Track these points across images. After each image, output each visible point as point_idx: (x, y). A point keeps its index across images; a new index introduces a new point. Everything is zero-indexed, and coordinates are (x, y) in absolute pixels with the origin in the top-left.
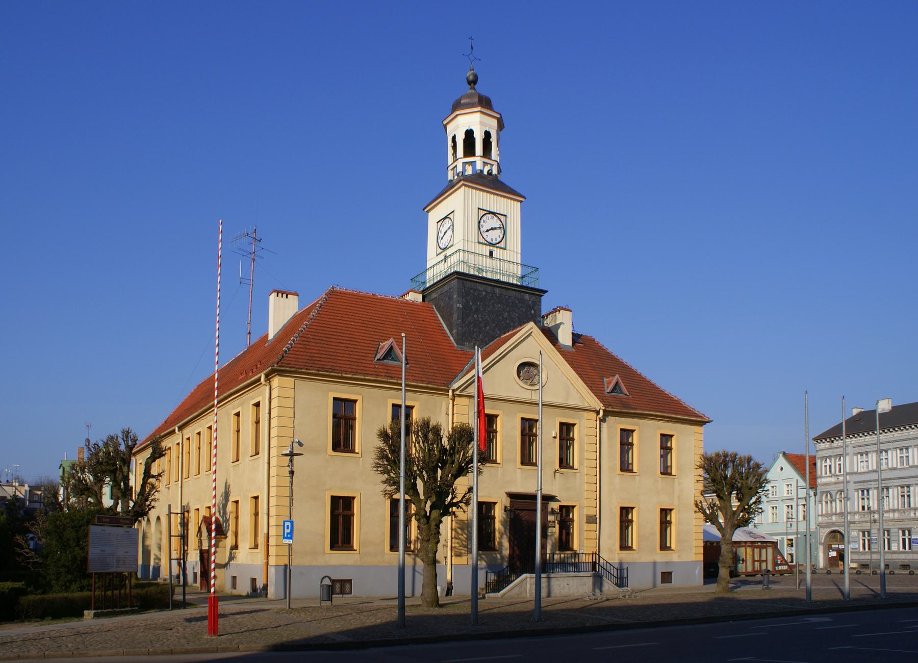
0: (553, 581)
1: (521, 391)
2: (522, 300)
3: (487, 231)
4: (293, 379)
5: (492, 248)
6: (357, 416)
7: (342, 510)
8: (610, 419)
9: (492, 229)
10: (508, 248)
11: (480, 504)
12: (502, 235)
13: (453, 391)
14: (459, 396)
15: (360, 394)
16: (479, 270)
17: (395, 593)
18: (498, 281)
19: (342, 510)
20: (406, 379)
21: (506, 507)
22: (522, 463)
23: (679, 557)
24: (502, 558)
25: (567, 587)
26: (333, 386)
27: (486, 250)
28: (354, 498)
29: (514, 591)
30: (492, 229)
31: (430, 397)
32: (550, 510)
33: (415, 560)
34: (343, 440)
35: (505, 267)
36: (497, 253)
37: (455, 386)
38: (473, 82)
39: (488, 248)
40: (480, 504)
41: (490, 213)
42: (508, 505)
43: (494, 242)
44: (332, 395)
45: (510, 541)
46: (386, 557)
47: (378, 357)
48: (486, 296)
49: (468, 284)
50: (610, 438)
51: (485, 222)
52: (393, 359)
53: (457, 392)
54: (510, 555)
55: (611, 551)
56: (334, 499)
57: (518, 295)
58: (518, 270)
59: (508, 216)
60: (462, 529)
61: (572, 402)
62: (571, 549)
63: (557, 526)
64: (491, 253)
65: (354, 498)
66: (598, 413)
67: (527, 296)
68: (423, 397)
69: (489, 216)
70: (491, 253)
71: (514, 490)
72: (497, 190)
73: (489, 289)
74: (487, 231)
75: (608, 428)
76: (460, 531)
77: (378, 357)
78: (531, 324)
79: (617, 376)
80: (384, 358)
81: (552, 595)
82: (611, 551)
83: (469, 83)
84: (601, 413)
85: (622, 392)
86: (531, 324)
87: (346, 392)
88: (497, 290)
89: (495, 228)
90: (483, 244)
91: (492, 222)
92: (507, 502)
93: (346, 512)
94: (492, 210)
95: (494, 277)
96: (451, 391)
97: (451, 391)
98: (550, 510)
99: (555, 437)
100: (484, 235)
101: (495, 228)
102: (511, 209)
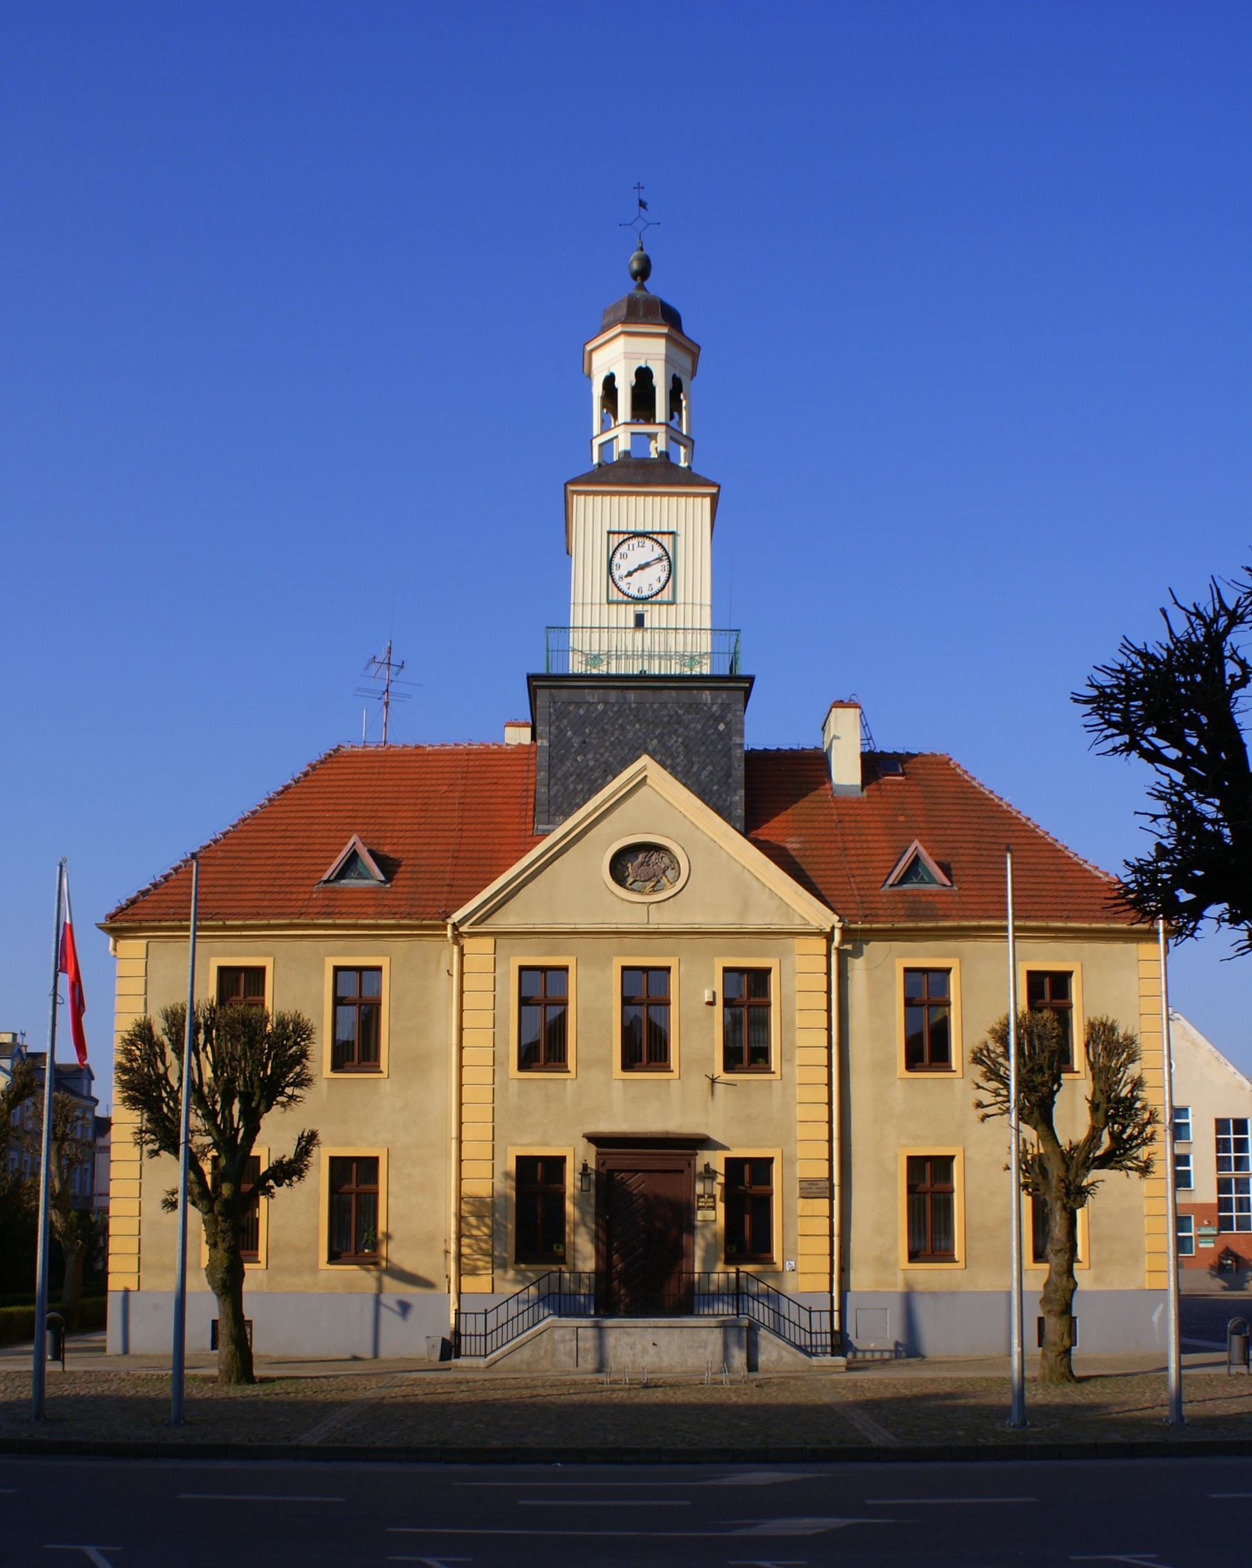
0: (612, 1338)
1: (625, 908)
2: (694, 707)
3: (630, 574)
4: (144, 942)
5: (639, 608)
6: (952, 999)
7: (929, 1181)
8: (874, 949)
9: (641, 567)
10: (680, 599)
11: (338, 1164)
12: (664, 576)
13: (455, 927)
14: (472, 935)
15: (267, 954)
16: (595, 659)
17: (168, 1346)
18: (643, 677)
19: (929, 1181)
20: (1015, 918)
21: (585, 1167)
22: (627, 1065)
23: (1097, 1279)
24: (577, 1275)
25: (652, 1350)
26: (219, 945)
27: (626, 615)
28: (952, 1158)
29: (517, 1357)
30: (641, 567)
31: (415, 943)
32: (700, 1168)
33: (379, 1280)
34: (927, 1048)
35: (677, 643)
36: (653, 616)
37: (457, 916)
38: (643, 273)
39: (631, 610)
40: (338, 1164)
41: (636, 535)
42: (592, 1165)
43: (646, 593)
44: (901, 964)
45: (596, 1239)
46: (322, 1275)
47: (890, 881)
48: (604, 712)
49: (564, 695)
50: (877, 991)
51: (623, 556)
52: (922, 881)
53: (463, 929)
54: (597, 1272)
55: (883, 1263)
56: (916, 1164)
57: (684, 695)
58: (704, 643)
59: (681, 532)
60: (480, 1217)
61: (755, 921)
62: (770, 1261)
63: (721, 1206)
64: (640, 620)
65: (952, 1158)
66: (829, 937)
67: (707, 696)
68: (400, 946)
69: (635, 541)
70: (640, 620)
71: (605, 1126)
72: (647, 484)
73: (613, 696)
74: (630, 574)
75: (869, 969)
76: (473, 1220)
77: (890, 881)
78: (645, 760)
79: (916, 843)
80: (341, 874)
81: (612, 1364)
82: (883, 1263)
83: (635, 276)
84: (837, 936)
85: (933, 880)
86: (645, 760)
87: (926, 955)
88: (632, 696)
89: (647, 565)
90: (618, 603)
91: (645, 551)
92: (589, 1155)
93: (939, 1186)
94: (640, 529)
95: (634, 668)
96: (449, 927)
97: (449, 927)
98: (700, 1168)
99: (712, 1004)
100: (623, 585)
101: (647, 565)
102: (687, 515)
